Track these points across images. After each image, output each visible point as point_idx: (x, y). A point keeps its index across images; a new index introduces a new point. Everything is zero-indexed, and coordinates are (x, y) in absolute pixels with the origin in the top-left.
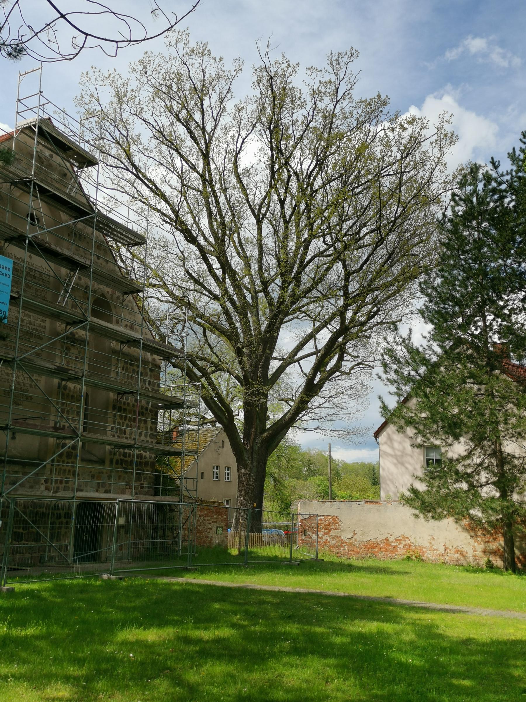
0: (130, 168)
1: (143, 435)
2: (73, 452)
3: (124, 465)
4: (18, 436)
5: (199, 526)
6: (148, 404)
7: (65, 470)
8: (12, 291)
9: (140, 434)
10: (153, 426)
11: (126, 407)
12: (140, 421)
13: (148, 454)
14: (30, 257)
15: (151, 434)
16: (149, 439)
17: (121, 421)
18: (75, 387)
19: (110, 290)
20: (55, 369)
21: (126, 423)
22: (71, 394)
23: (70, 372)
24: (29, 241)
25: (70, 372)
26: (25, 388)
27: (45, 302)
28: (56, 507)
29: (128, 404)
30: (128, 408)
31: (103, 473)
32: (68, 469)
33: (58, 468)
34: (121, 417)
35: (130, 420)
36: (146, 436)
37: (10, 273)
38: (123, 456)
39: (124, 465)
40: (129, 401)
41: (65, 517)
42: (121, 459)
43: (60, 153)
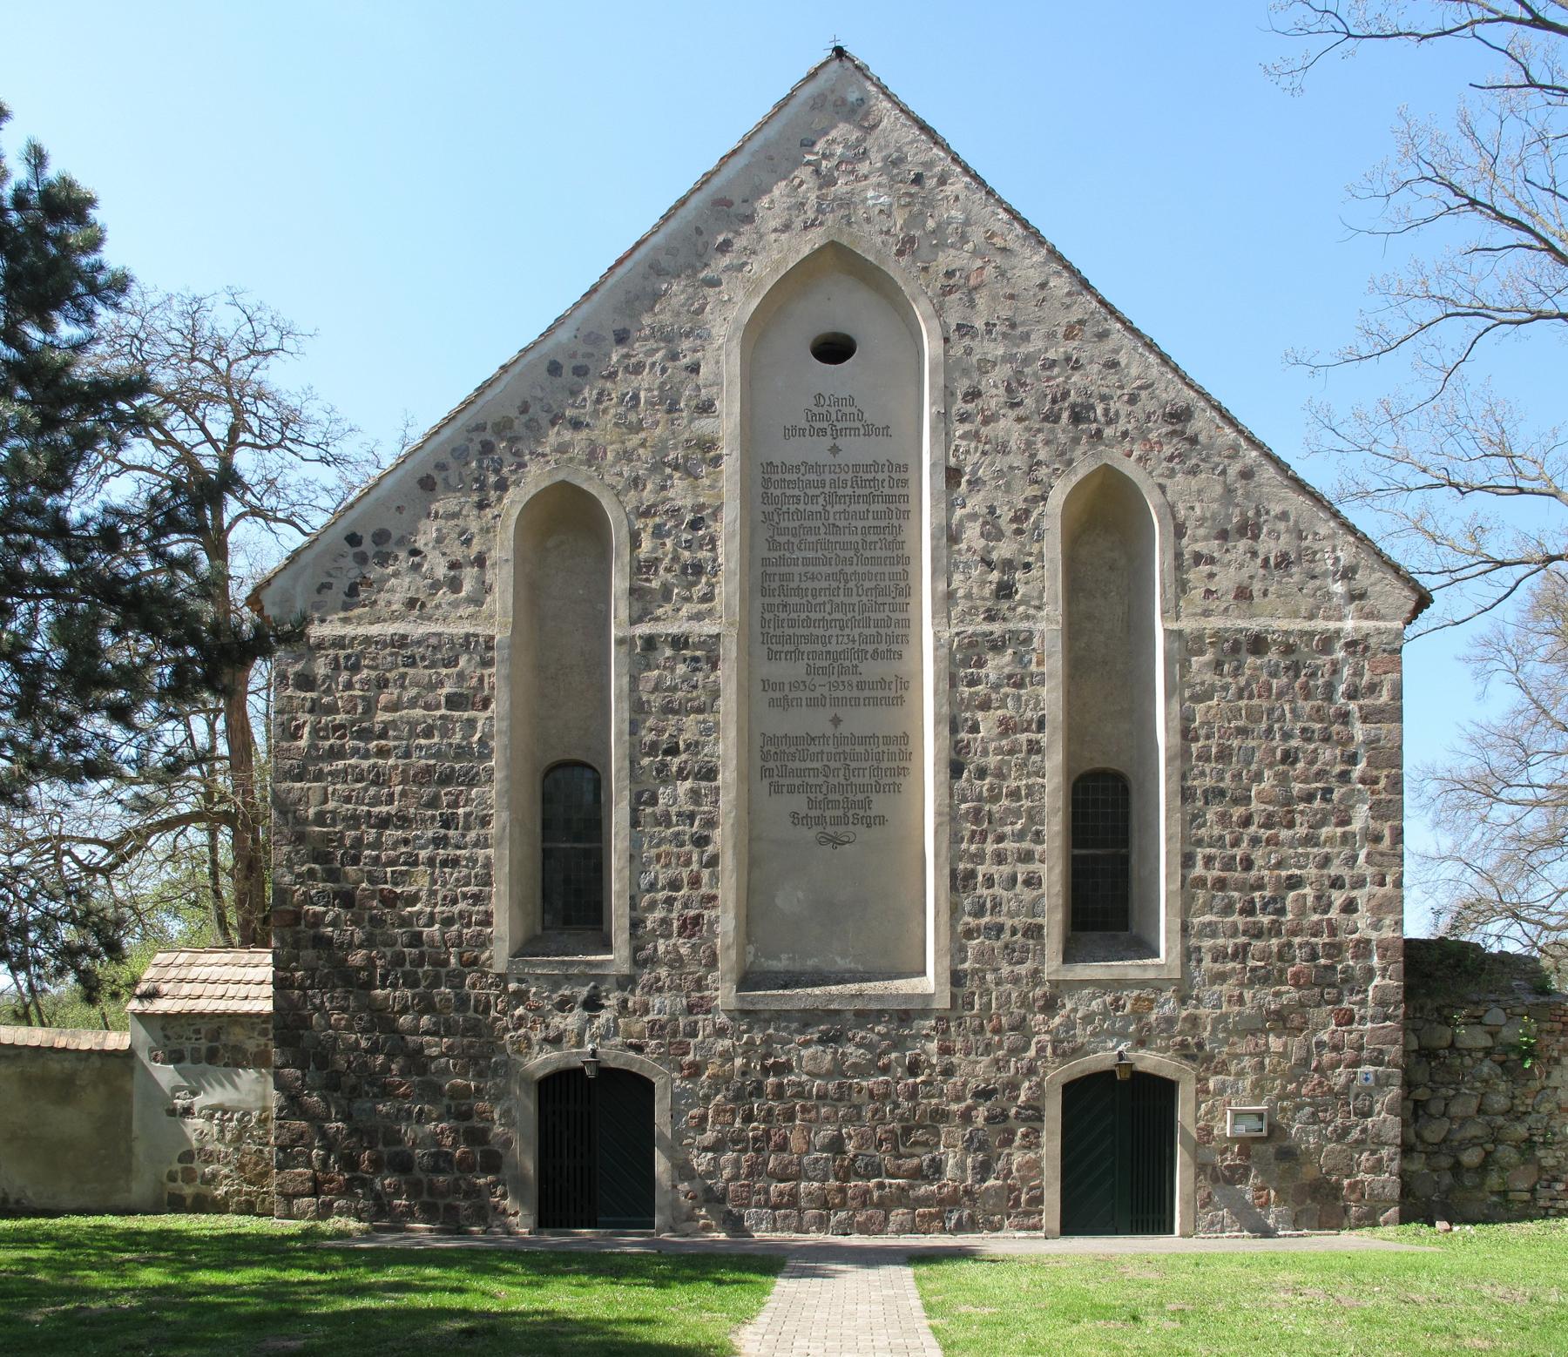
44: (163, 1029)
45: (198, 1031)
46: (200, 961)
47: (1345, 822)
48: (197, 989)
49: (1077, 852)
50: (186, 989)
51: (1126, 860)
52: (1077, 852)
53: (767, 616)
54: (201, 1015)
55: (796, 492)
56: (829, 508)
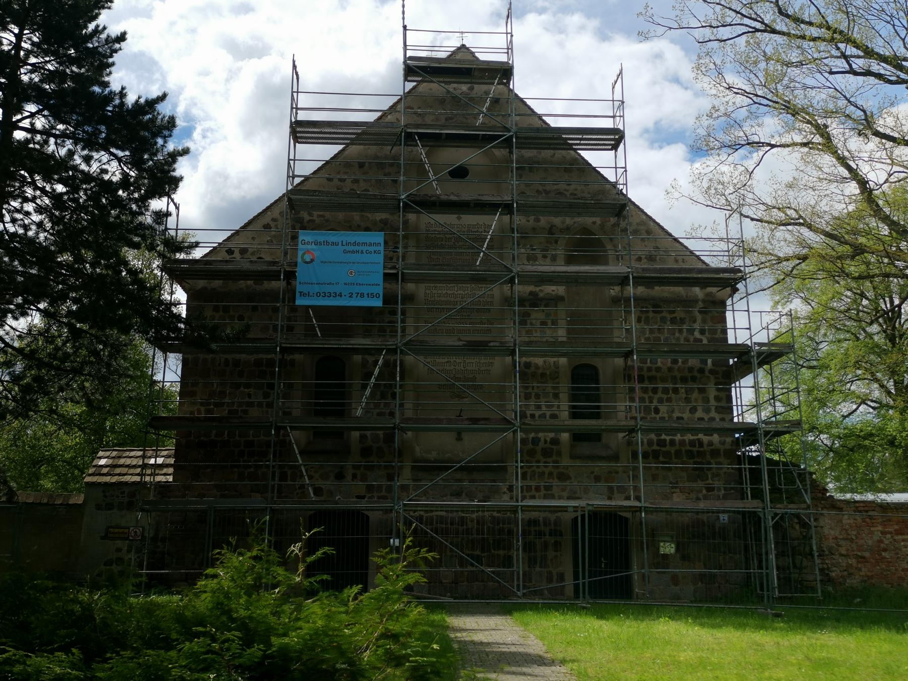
0: (780, 26)
1: (700, 409)
2: (554, 447)
3: (661, 459)
4: (466, 437)
5: (885, 550)
6: (705, 362)
7: (543, 473)
8: (385, 267)
9: (693, 410)
10: (723, 395)
11: (653, 373)
12: (689, 391)
13: (716, 438)
14: (459, 218)
15: (717, 407)
16: (713, 414)
17: (646, 396)
18: (545, 362)
19: (598, 220)
20: (464, 345)
21: (656, 396)
22: (540, 371)
23: (492, 344)
24: (403, 202)
25: (492, 344)
26: (471, 376)
27: (437, 267)
28: (463, 520)
29: (658, 369)
30: (659, 375)
31: (617, 472)
32: (547, 471)
33: (529, 471)
34: (645, 390)
35: (666, 391)
36: (707, 411)
37: (382, 248)
38: (658, 445)
39: (661, 459)
40: (659, 364)
41: (550, 535)
42: (653, 451)
43: (434, 80)
44: (104, 492)
45: (123, 493)
46: (124, 455)
47: (390, 478)
48: (125, 470)
49: (529, 478)
50: (118, 471)
51: (367, 574)
52: (529, 478)
53: (427, 291)
54: (126, 483)
55: (442, 236)
56: (456, 243)
